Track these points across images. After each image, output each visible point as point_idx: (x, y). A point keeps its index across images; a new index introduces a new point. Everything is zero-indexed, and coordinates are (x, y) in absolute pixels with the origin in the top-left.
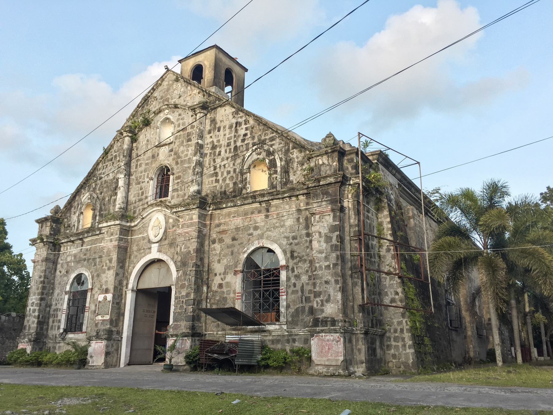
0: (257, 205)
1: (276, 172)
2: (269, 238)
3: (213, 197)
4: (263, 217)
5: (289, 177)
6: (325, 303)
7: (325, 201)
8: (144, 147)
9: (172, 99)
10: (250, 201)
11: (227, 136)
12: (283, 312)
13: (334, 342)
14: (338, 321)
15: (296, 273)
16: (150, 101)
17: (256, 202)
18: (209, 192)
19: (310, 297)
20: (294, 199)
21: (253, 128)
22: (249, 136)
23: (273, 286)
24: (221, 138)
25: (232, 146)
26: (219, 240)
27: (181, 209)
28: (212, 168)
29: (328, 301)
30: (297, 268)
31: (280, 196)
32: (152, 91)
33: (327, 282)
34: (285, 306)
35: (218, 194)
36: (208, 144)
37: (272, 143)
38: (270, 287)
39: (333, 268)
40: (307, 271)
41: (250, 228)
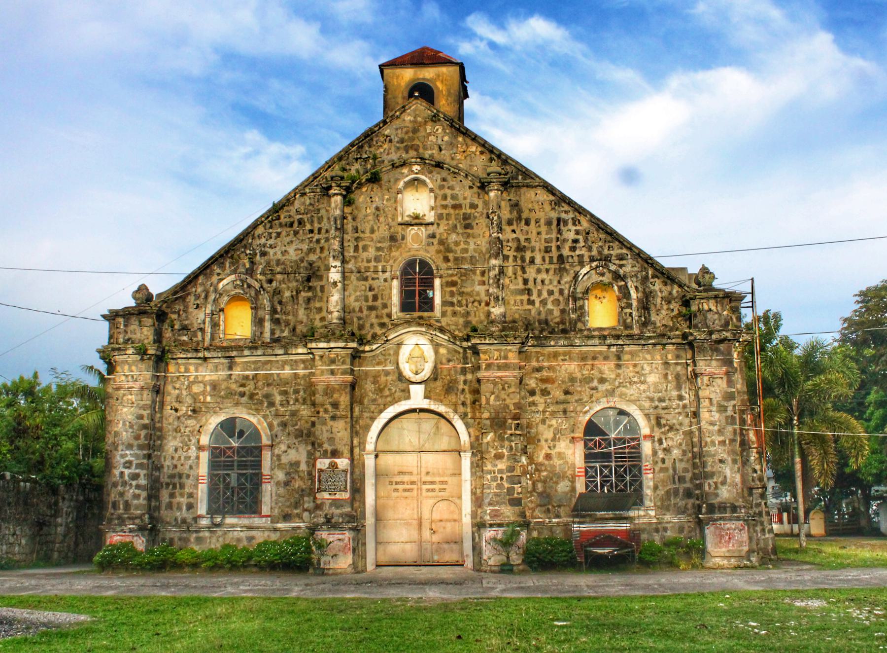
0: (604, 348)
1: (630, 306)
2: (623, 397)
3: (527, 326)
4: (613, 366)
5: (650, 315)
6: (719, 485)
7: (715, 359)
8: (370, 218)
9: (425, 148)
10: (597, 341)
11: (544, 236)
12: (649, 494)
13: (737, 531)
14: (740, 507)
15: (665, 445)
16: (375, 139)
17: (604, 344)
18: (517, 316)
19: (685, 476)
20: (659, 347)
21: (588, 233)
22: (582, 244)
23: (629, 461)
24: (533, 237)
25: (555, 254)
26: (542, 390)
27: (491, 342)
28: (520, 280)
29: (724, 483)
30: (666, 439)
31: (643, 342)
32: (381, 125)
33: (721, 461)
34: (652, 487)
35: (534, 322)
36: (508, 241)
37: (622, 262)
38: (625, 461)
39: (730, 444)
40: (681, 444)
41: (593, 379)
